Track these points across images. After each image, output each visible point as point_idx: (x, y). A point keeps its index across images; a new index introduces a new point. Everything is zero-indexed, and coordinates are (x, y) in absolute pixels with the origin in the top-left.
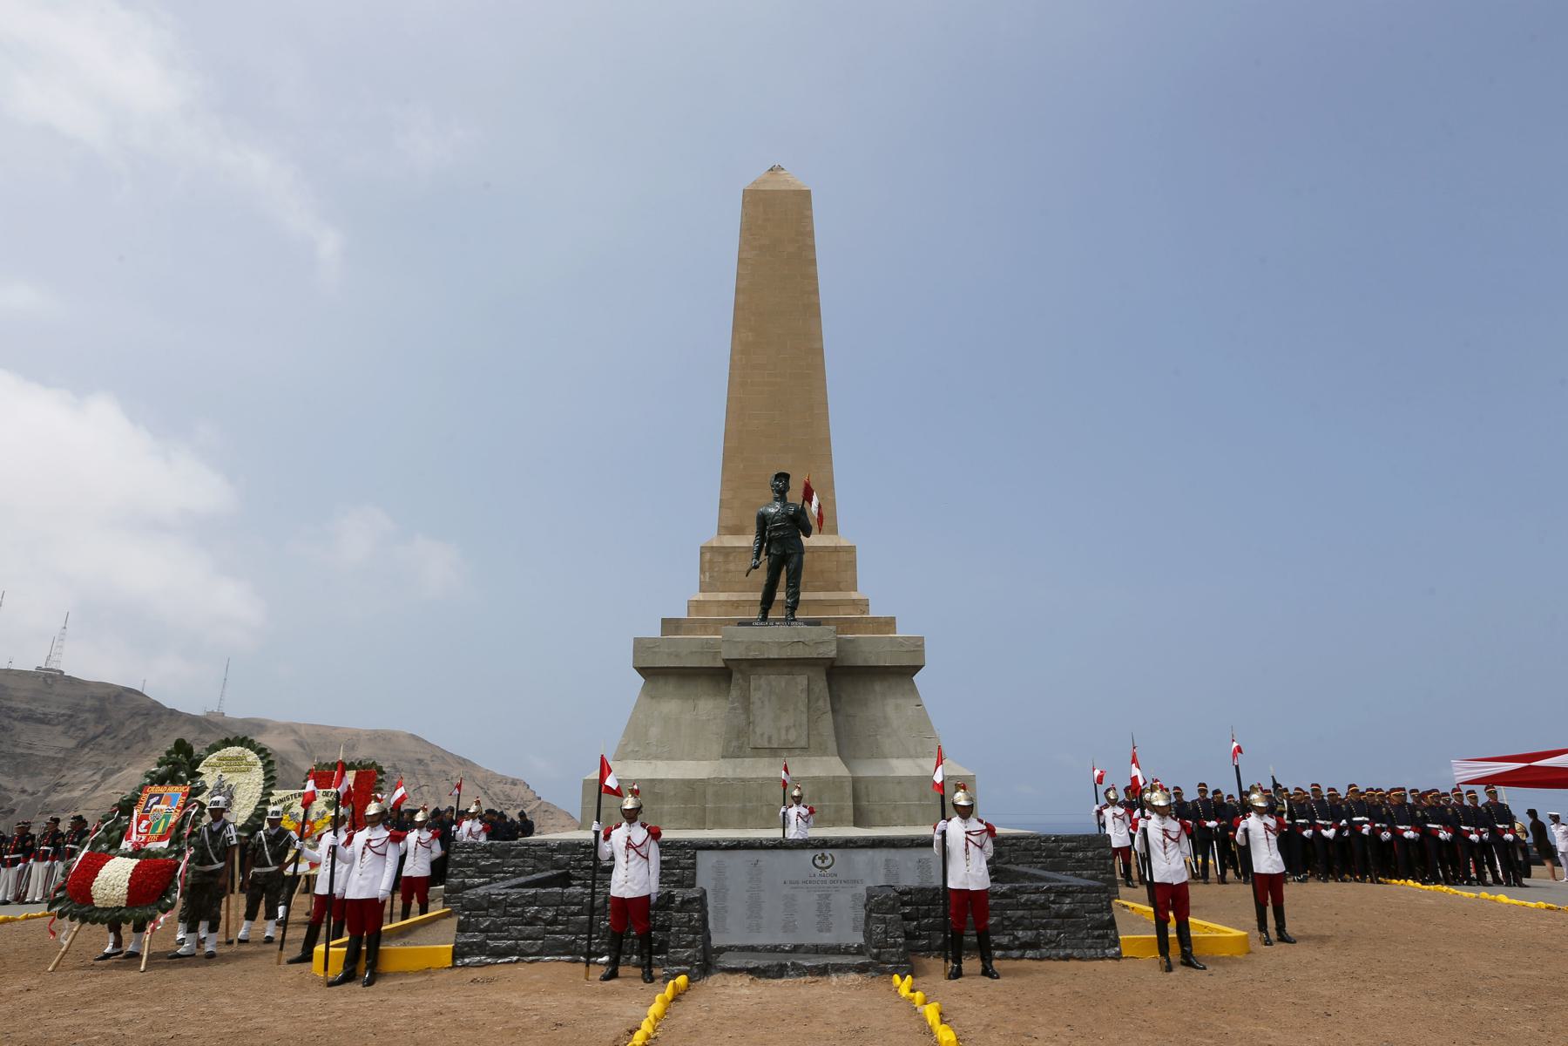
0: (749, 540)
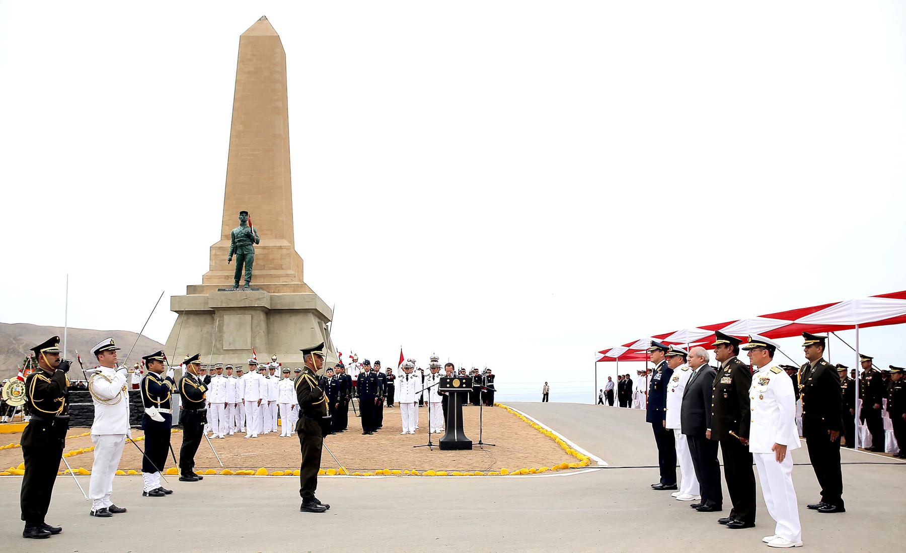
0: (229, 244)
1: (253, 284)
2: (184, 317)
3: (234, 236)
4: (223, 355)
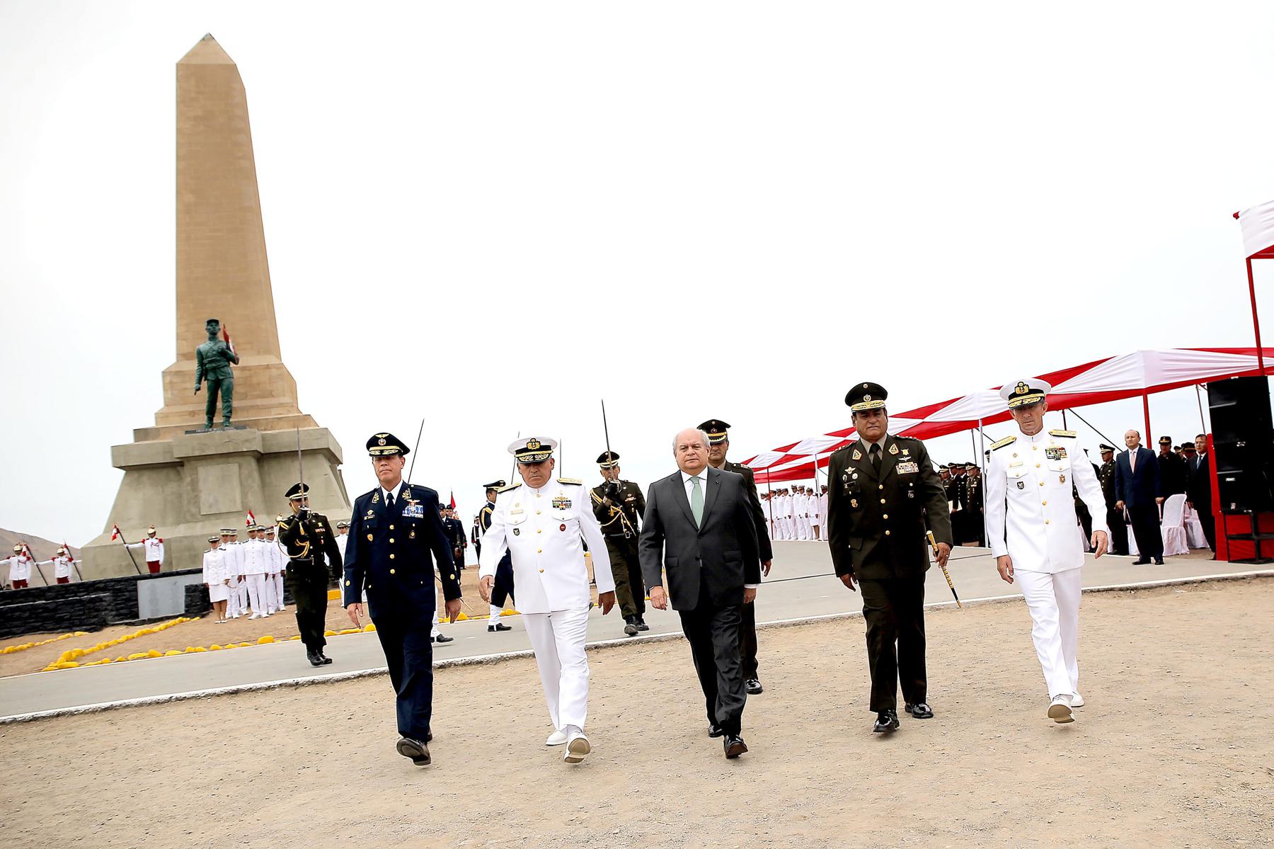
0: (194, 366)
1: (236, 420)
2: (135, 475)
3: (201, 356)
4: (201, 523)
